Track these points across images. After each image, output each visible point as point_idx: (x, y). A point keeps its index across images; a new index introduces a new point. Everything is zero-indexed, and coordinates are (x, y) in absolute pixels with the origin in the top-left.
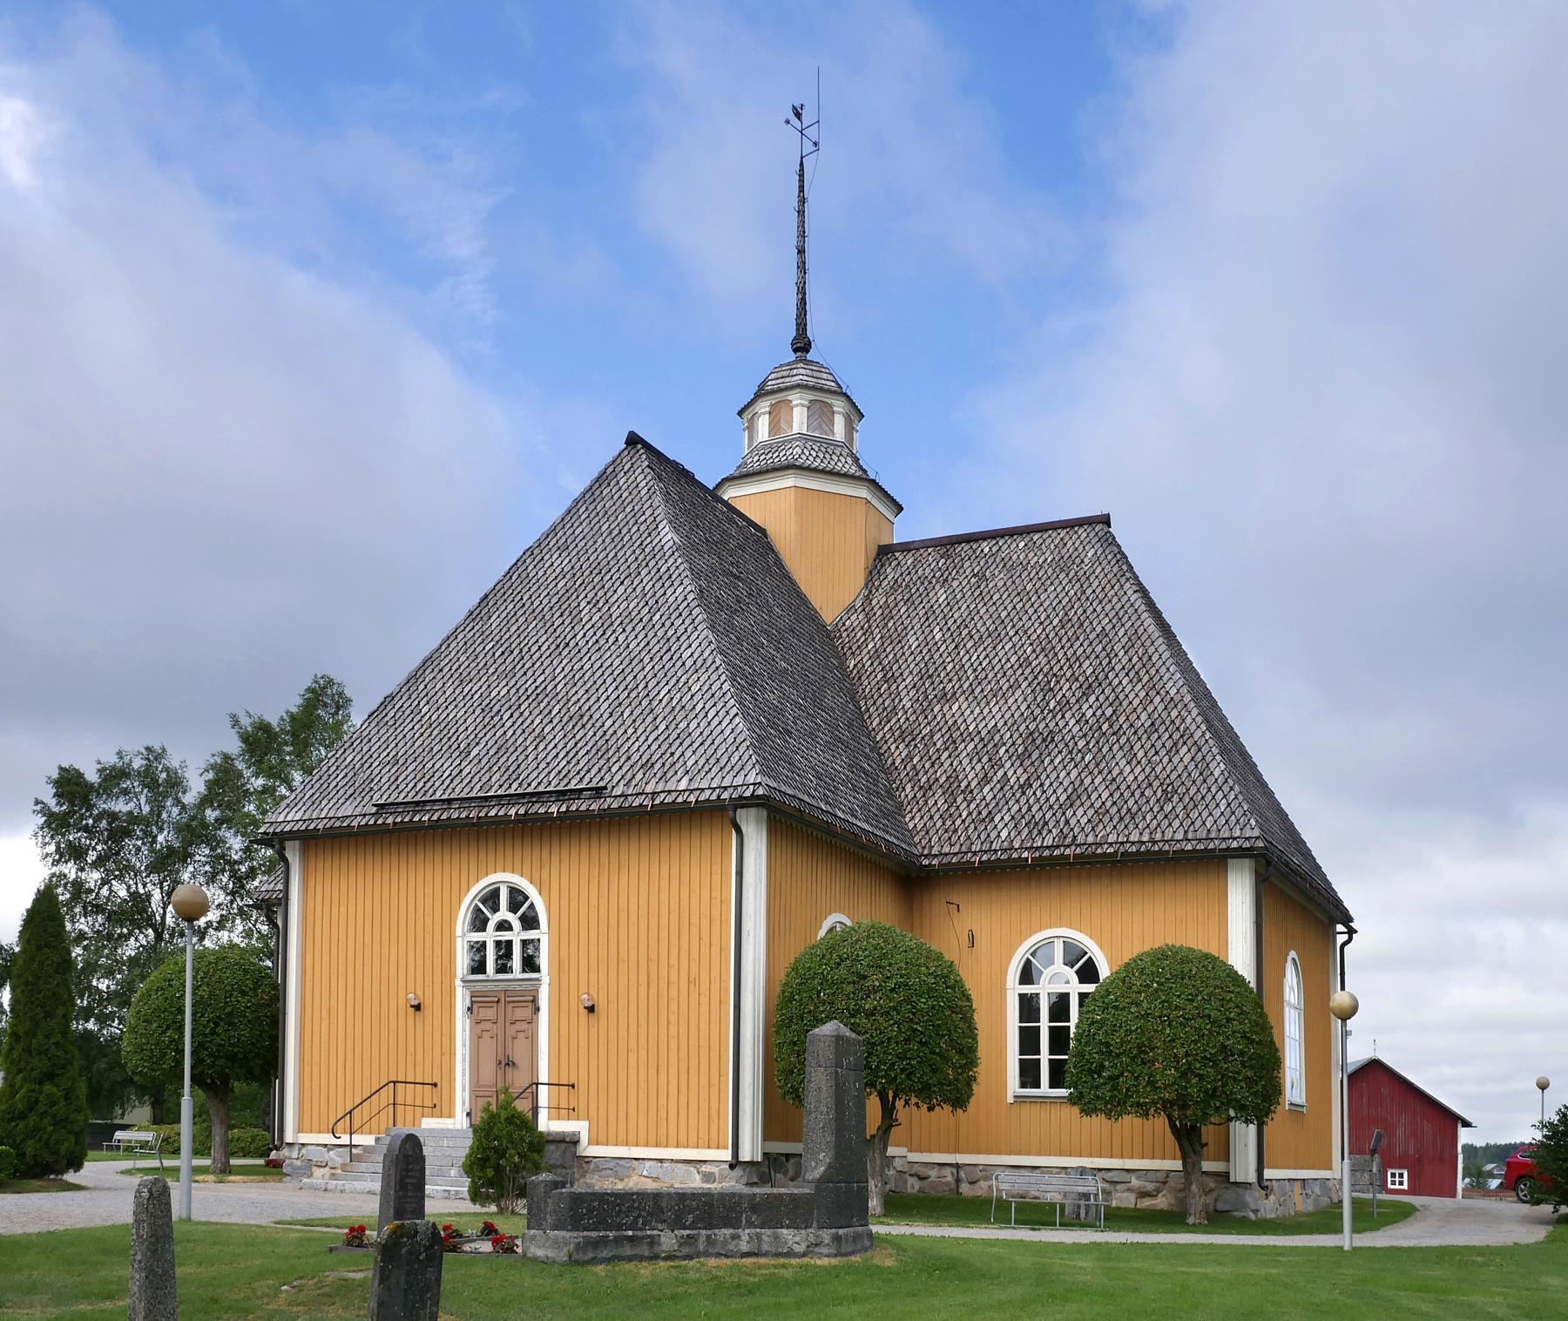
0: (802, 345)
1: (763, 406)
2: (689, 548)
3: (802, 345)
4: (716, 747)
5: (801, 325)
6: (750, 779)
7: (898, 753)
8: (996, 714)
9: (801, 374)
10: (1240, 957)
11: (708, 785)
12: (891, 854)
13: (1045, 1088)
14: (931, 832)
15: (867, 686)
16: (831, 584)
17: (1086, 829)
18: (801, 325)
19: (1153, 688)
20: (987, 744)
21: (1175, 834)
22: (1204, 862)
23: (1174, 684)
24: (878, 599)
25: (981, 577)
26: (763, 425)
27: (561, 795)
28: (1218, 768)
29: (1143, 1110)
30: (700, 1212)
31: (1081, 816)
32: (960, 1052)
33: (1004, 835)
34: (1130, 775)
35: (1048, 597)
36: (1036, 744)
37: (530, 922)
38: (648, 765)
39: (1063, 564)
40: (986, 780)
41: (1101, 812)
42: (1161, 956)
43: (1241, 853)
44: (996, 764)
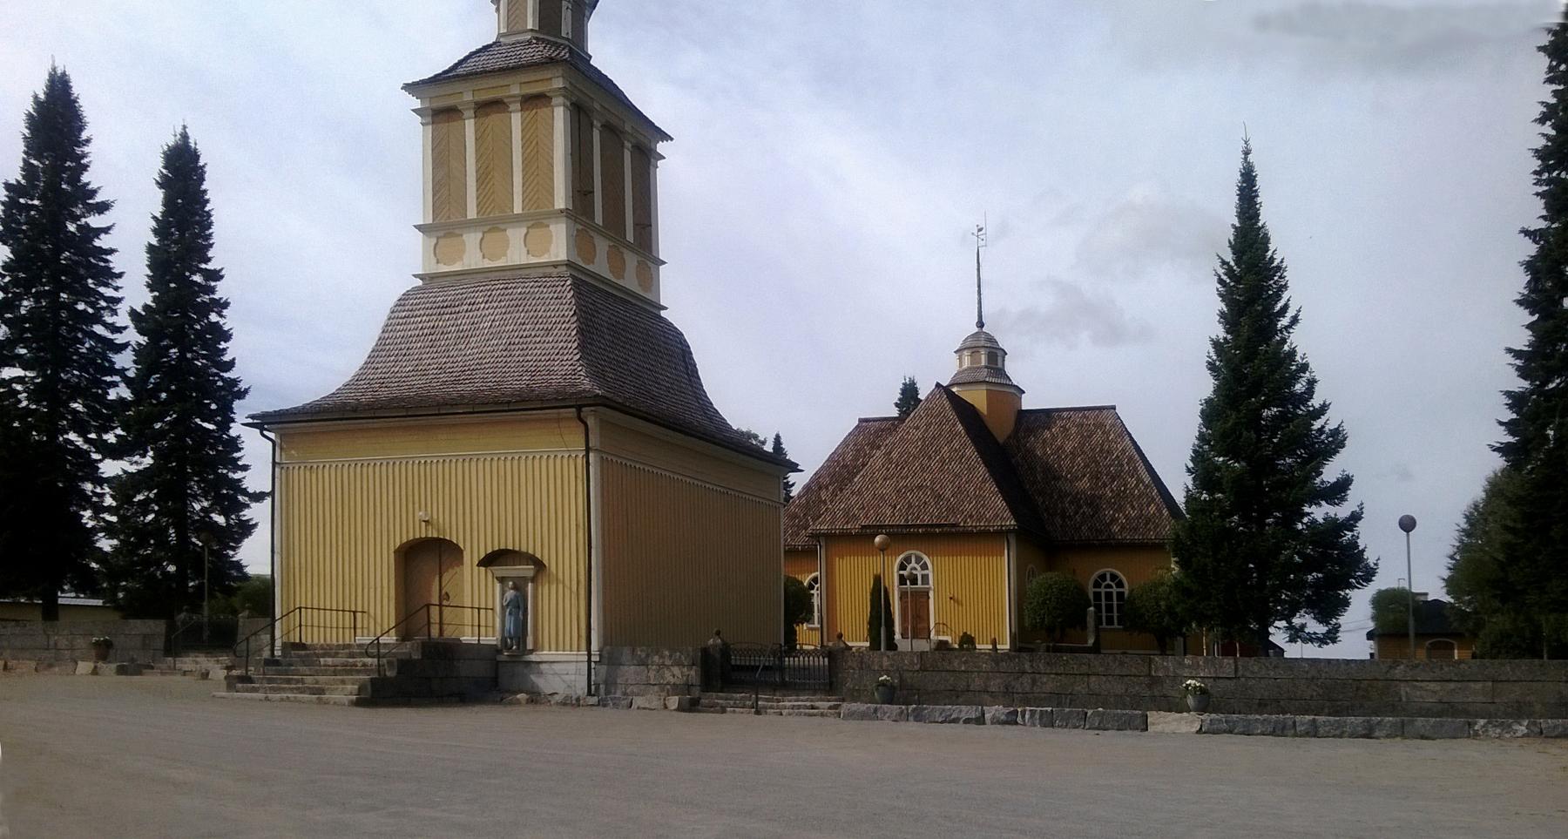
2: (968, 432)
4: (997, 510)
5: (980, 316)
18: (980, 316)
23: (1147, 479)
37: (925, 567)
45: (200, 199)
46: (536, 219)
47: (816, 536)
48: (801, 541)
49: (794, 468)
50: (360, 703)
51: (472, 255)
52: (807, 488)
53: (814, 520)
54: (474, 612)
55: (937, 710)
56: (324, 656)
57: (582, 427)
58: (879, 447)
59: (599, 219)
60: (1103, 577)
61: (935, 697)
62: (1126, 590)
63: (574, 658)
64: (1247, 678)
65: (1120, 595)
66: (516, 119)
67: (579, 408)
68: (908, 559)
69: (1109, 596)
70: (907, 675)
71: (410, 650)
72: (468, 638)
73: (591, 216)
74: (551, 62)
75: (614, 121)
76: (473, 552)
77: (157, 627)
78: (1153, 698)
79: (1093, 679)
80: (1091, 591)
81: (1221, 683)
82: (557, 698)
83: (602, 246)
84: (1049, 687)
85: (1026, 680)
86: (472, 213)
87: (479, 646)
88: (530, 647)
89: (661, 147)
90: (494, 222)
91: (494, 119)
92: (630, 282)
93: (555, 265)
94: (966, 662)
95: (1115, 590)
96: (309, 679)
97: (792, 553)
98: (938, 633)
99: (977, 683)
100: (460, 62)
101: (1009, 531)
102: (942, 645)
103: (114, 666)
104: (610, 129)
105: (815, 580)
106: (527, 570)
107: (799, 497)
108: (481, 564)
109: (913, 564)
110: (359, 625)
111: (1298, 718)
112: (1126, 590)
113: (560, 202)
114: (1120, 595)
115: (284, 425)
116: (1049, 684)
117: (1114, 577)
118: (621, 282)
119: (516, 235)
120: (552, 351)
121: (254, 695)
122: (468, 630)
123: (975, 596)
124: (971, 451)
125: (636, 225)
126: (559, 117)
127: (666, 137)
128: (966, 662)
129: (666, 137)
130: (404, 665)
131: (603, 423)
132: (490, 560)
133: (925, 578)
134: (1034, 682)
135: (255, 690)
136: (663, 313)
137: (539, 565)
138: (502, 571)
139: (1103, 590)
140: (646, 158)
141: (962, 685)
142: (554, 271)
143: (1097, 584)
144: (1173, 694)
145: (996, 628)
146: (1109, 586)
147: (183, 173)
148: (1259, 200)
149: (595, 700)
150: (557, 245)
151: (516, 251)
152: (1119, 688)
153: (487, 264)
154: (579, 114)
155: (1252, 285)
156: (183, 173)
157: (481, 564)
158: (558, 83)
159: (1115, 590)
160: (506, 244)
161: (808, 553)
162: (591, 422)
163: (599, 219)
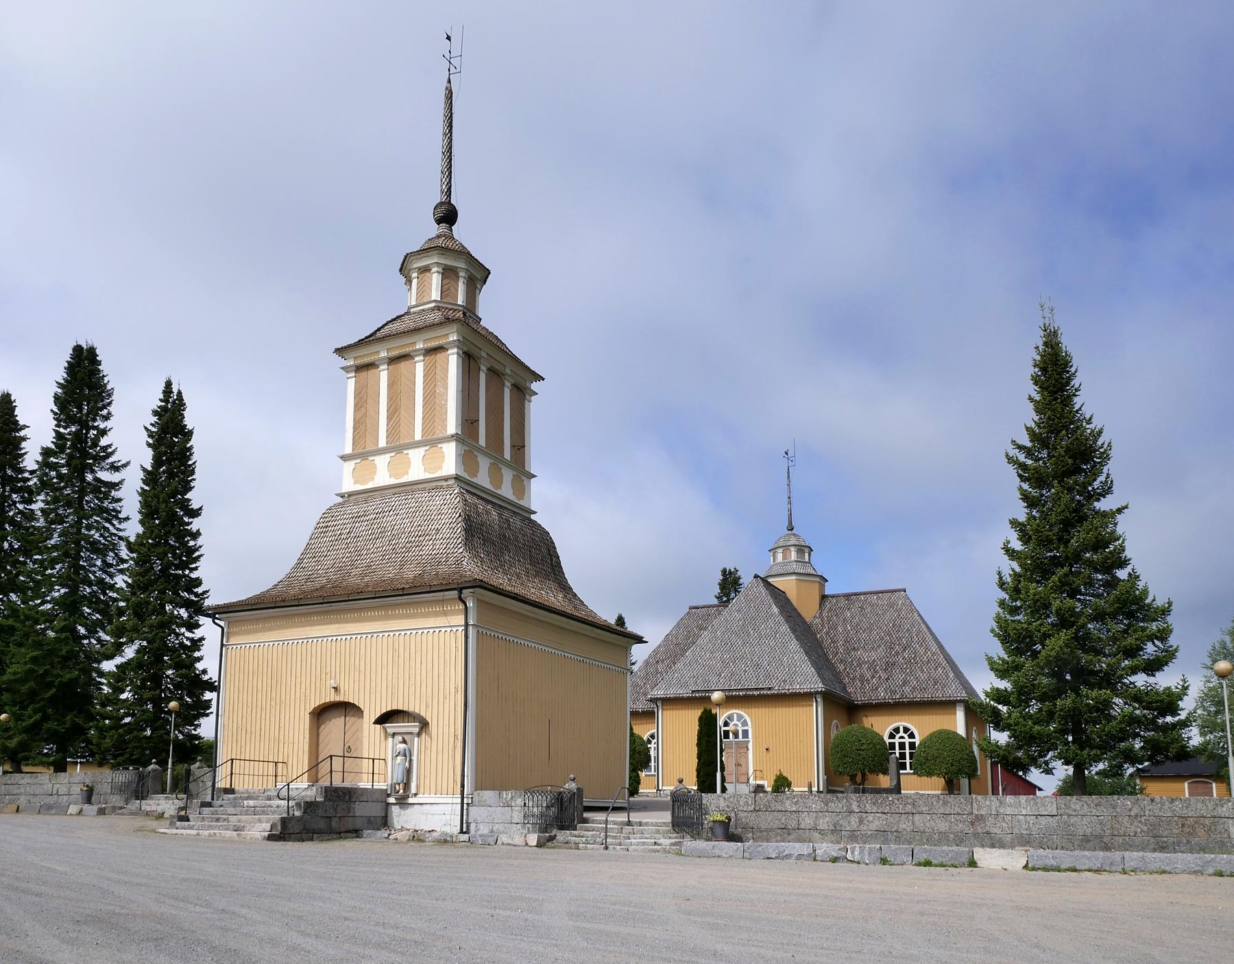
0: (448, 216)
1: (780, 550)
2: (781, 612)
3: (448, 216)
4: (808, 678)
5: (790, 522)
6: (820, 686)
7: (841, 667)
8: (874, 655)
9: (793, 541)
10: (961, 731)
11: (806, 688)
12: (841, 698)
13: (908, 770)
14: (858, 694)
15: (826, 644)
16: (808, 609)
17: (909, 693)
18: (790, 522)
19: (927, 649)
20: (872, 665)
21: (939, 695)
22: (948, 705)
23: (934, 648)
24: (825, 614)
25: (862, 608)
26: (780, 557)
27: (757, 689)
28: (952, 675)
29: (938, 775)
30: (445, 841)
31: (907, 689)
32: (157, 679)
33: (882, 695)
34: (923, 676)
35: (887, 616)
36: (889, 666)
37: (745, 723)
38: (785, 681)
39: (891, 605)
40: (873, 677)
41: (914, 688)
42: (940, 732)
43: (960, 701)
44: (877, 672)
45: (184, 454)
46: (431, 442)
47: (654, 700)
48: (641, 706)
49: (639, 640)
50: (271, 838)
51: (382, 473)
52: (647, 663)
53: (652, 689)
54: (373, 761)
55: (771, 848)
56: (247, 798)
57: (461, 607)
58: (706, 628)
59: (482, 441)
60: (897, 730)
61: (764, 835)
62: (917, 741)
63: (450, 801)
64: (1069, 816)
65: (912, 745)
66: (420, 368)
67: (460, 590)
68: (730, 717)
69: (902, 746)
70: (742, 815)
71: (313, 794)
72: (365, 784)
73: (477, 440)
74: (448, 321)
75: (497, 367)
76: (372, 711)
77: (123, 776)
78: (976, 835)
79: (917, 817)
80: (888, 741)
81: (1043, 821)
82: (434, 834)
83: (484, 463)
84: (874, 826)
85: (854, 820)
86: (382, 443)
87: (372, 791)
88: (413, 790)
89: (535, 386)
90: (397, 447)
91: (404, 365)
92: (506, 491)
93: (446, 479)
94: (796, 803)
95: (907, 740)
96: (233, 818)
97: (635, 714)
98: (756, 778)
99: (807, 821)
100: (379, 329)
101: (817, 693)
102: (759, 789)
103: (95, 808)
104: (494, 373)
105: (652, 736)
106: (414, 727)
107: (640, 670)
108: (377, 722)
109: (735, 721)
110: (279, 773)
111: (1127, 854)
112: (917, 741)
113: (452, 425)
114: (912, 745)
115: (234, 613)
116: (875, 822)
117: (906, 730)
118: (499, 492)
119: (416, 456)
120: (440, 538)
121: (189, 831)
122: (365, 777)
123: (782, 745)
124: (785, 628)
125: (513, 446)
126: (453, 361)
127: (539, 378)
128: (796, 803)
129: (539, 378)
130: (309, 806)
131: (480, 602)
132: (384, 719)
133: (745, 733)
134: (861, 822)
135: (191, 828)
136: (533, 517)
137: (424, 725)
138: (391, 727)
139: (897, 741)
140: (522, 393)
141: (793, 824)
142: (445, 484)
143: (892, 736)
144: (995, 831)
145: (808, 771)
146: (902, 737)
147: (170, 433)
148: (1075, 382)
149: (465, 837)
150: (448, 461)
151: (417, 467)
152: (942, 826)
153: (393, 481)
154: (469, 360)
155: (1063, 460)
156: (170, 433)
157: (377, 722)
158: (453, 337)
159: (907, 740)
160: (408, 464)
161: (649, 715)
162: (470, 604)
163: (482, 441)
